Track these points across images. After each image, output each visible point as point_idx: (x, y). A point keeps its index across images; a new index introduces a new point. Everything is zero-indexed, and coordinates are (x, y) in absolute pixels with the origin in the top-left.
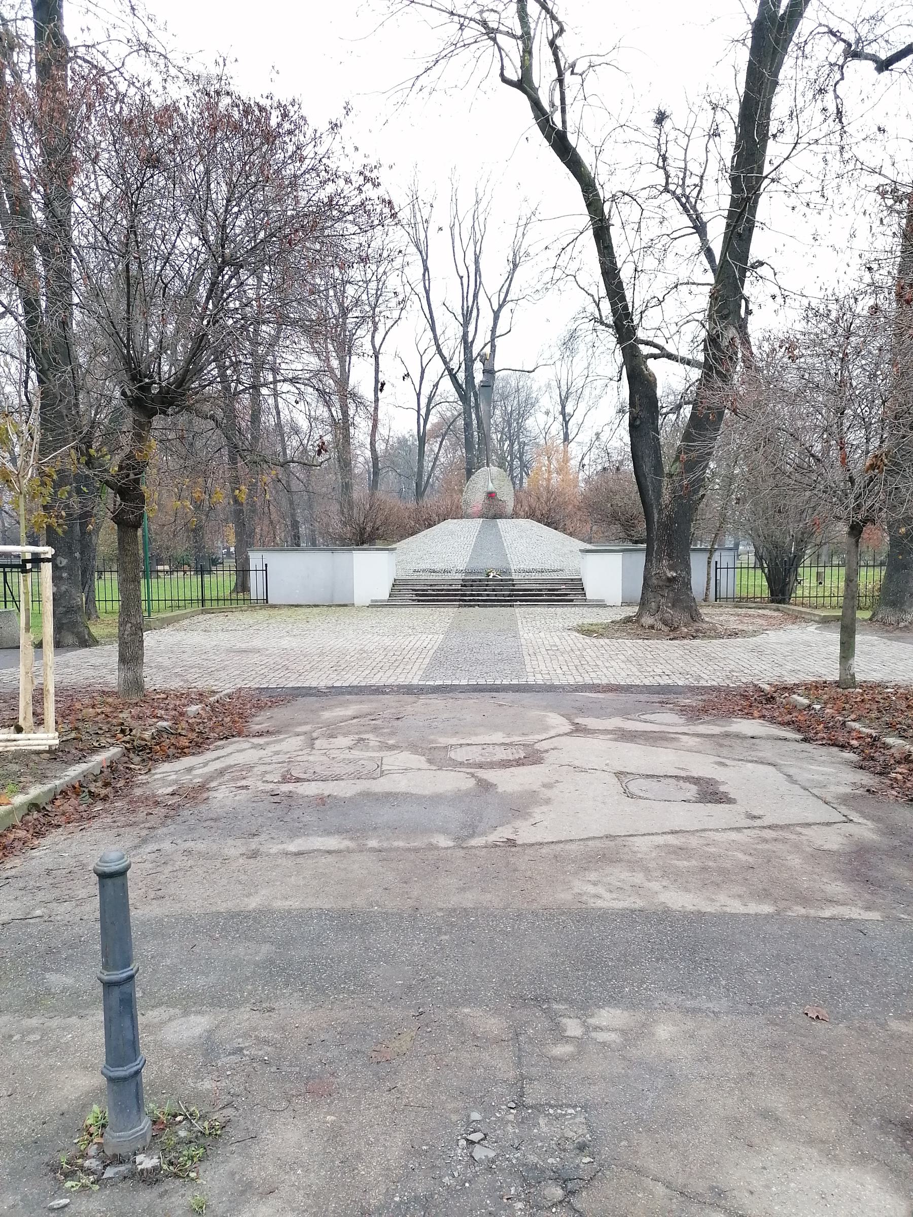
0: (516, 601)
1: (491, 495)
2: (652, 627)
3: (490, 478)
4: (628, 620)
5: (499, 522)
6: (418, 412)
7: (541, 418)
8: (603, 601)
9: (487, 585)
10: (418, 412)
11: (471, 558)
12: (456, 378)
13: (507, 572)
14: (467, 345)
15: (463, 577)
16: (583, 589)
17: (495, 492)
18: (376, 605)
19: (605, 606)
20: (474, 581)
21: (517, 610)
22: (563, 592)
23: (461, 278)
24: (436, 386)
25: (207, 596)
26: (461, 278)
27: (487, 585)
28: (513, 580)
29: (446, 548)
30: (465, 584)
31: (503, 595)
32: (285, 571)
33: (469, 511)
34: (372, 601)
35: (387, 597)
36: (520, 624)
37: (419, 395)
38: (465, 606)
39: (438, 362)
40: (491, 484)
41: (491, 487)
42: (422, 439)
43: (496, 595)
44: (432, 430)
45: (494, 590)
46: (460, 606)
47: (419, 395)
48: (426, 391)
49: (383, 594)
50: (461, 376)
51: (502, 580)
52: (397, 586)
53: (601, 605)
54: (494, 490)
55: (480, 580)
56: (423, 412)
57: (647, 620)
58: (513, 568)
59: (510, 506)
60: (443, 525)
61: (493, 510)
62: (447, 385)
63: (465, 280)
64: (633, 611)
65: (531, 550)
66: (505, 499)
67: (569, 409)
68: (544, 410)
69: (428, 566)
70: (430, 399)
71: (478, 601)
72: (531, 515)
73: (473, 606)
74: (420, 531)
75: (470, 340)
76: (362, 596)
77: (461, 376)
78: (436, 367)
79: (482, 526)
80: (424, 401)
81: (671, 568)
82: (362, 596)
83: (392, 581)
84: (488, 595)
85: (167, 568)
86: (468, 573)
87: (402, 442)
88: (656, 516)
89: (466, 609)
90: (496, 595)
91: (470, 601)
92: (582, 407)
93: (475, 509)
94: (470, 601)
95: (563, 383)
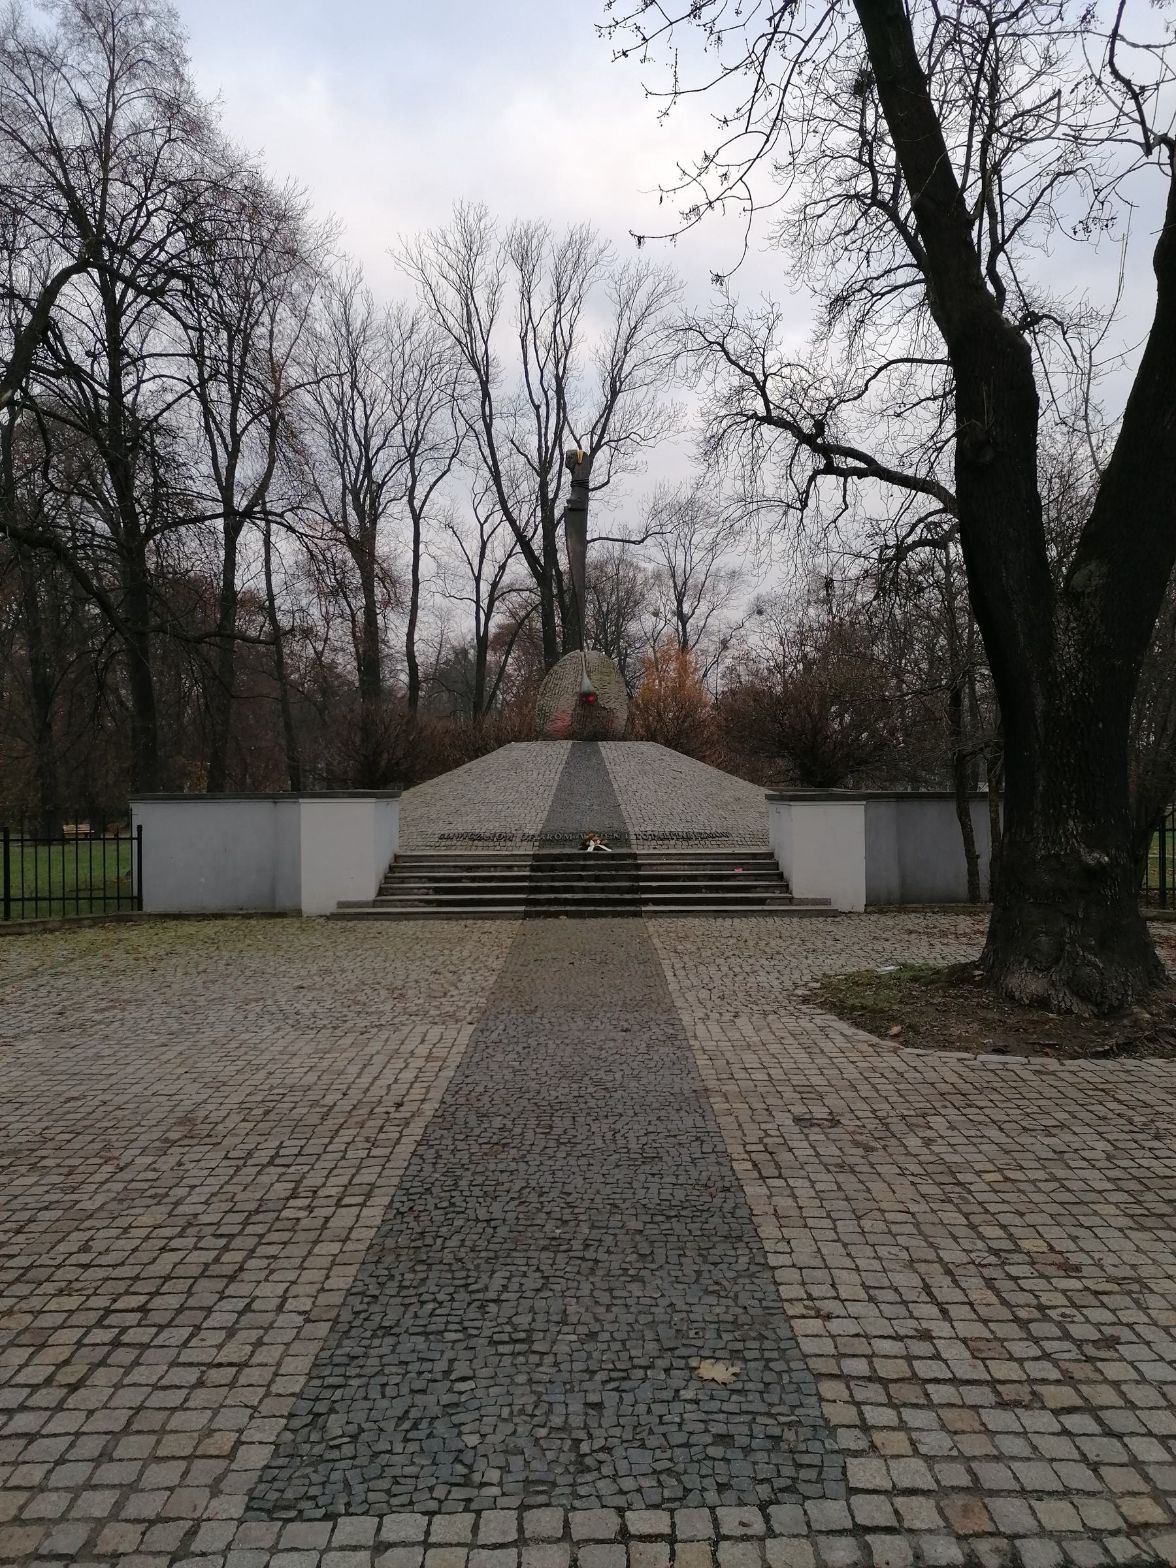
0: (646, 902)
1: (587, 700)
2: (1042, 1003)
3: (582, 671)
4: (959, 975)
5: (607, 749)
6: (478, 603)
7: (648, 621)
8: (826, 902)
9: (584, 868)
10: (478, 603)
11: (552, 811)
12: (530, 548)
13: (620, 838)
14: (546, 504)
15: (536, 851)
16: (781, 876)
17: (593, 694)
18: (347, 914)
19: (835, 914)
20: (557, 857)
21: (652, 925)
22: (750, 883)
23: (537, 408)
24: (503, 568)
25: (15, 892)
26: (537, 408)
27: (584, 868)
28: (635, 856)
29: (508, 796)
30: (539, 863)
31: (618, 890)
32: (183, 841)
33: (549, 727)
34: (341, 905)
35: (370, 894)
36: (669, 974)
37: (478, 579)
38: (538, 915)
39: (506, 531)
40: (586, 680)
41: (587, 684)
42: (482, 642)
43: (602, 890)
44: (497, 636)
45: (597, 879)
46: (526, 915)
47: (478, 579)
48: (489, 571)
49: (365, 888)
50: (537, 544)
51: (612, 857)
52: (398, 872)
53: (823, 910)
54: (592, 689)
55: (569, 857)
56: (484, 604)
57: (1027, 982)
58: (633, 830)
59: (622, 715)
60: (501, 752)
61: (591, 725)
62: (519, 569)
63: (543, 411)
64: (959, 942)
65: (664, 797)
66: (611, 705)
67: (686, 608)
68: (651, 609)
69: (468, 828)
70: (495, 585)
71: (566, 902)
72: (651, 737)
73: (556, 915)
74: (458, 763)
75: (551, 495)
76: (318, 892)
77: (537, 544)
78: (505, 536)
79: (572, 754)
80: (485, 588)
81: (1094, 841)
82: (318, 892)
83: (386, 860)
84: (586, 890)
85: (85, 827)
86: (545, 839)
87: (461, 653)
88: (1040, 703)
89: (539, 923)
90: (602, 890)
91: (549, 902)
92: (703, 608)
93: (559, 723)
94: (549, 902)
95: (679, 571)
